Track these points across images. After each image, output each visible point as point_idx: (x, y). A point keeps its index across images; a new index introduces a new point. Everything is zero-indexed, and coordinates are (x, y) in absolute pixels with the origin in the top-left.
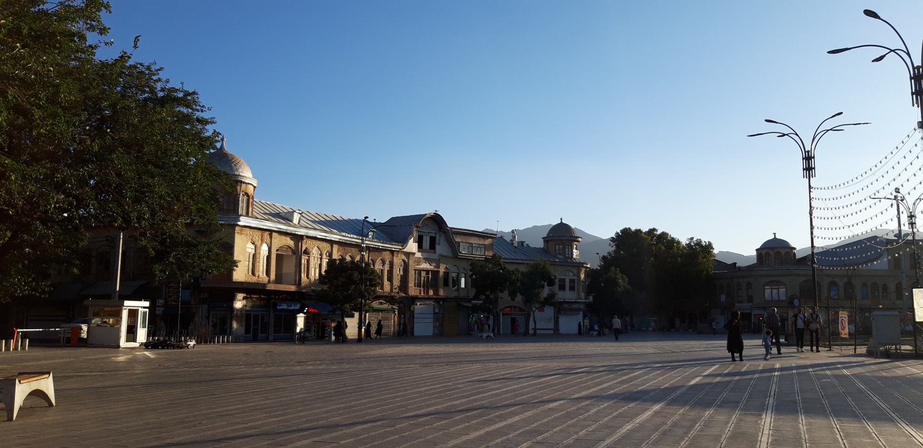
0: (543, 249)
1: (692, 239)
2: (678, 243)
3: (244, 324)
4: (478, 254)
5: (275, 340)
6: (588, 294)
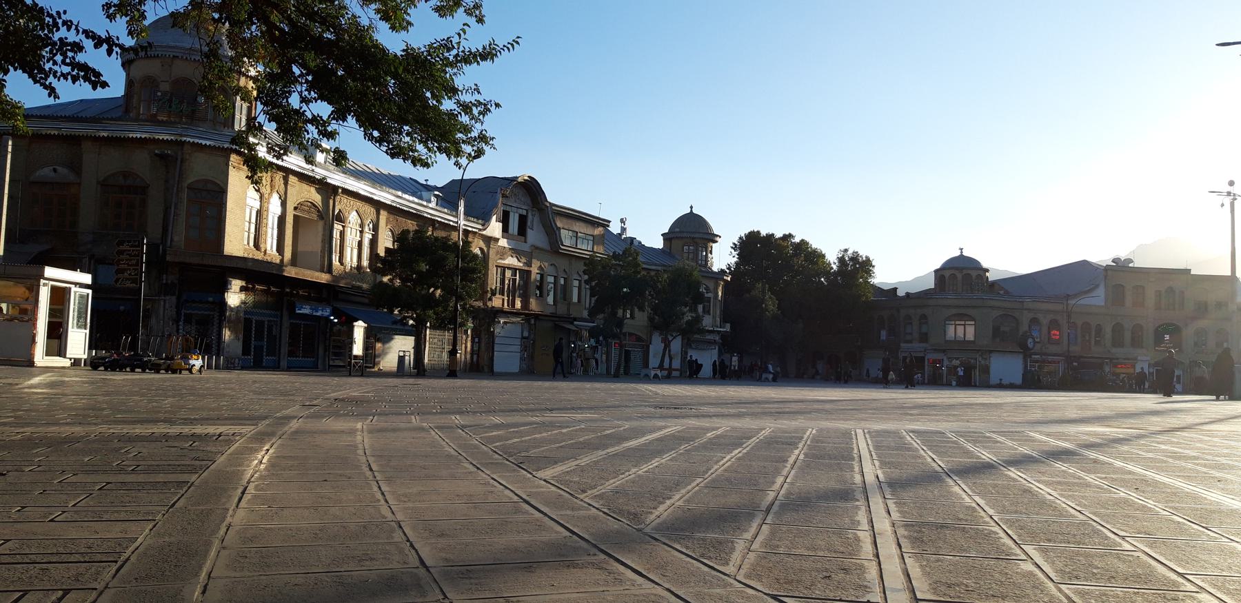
1: (846, 250)
2: (816, 257)
3: (241, 336)
4: (585, 247)
5: (290, 368)
6: (725, 320)
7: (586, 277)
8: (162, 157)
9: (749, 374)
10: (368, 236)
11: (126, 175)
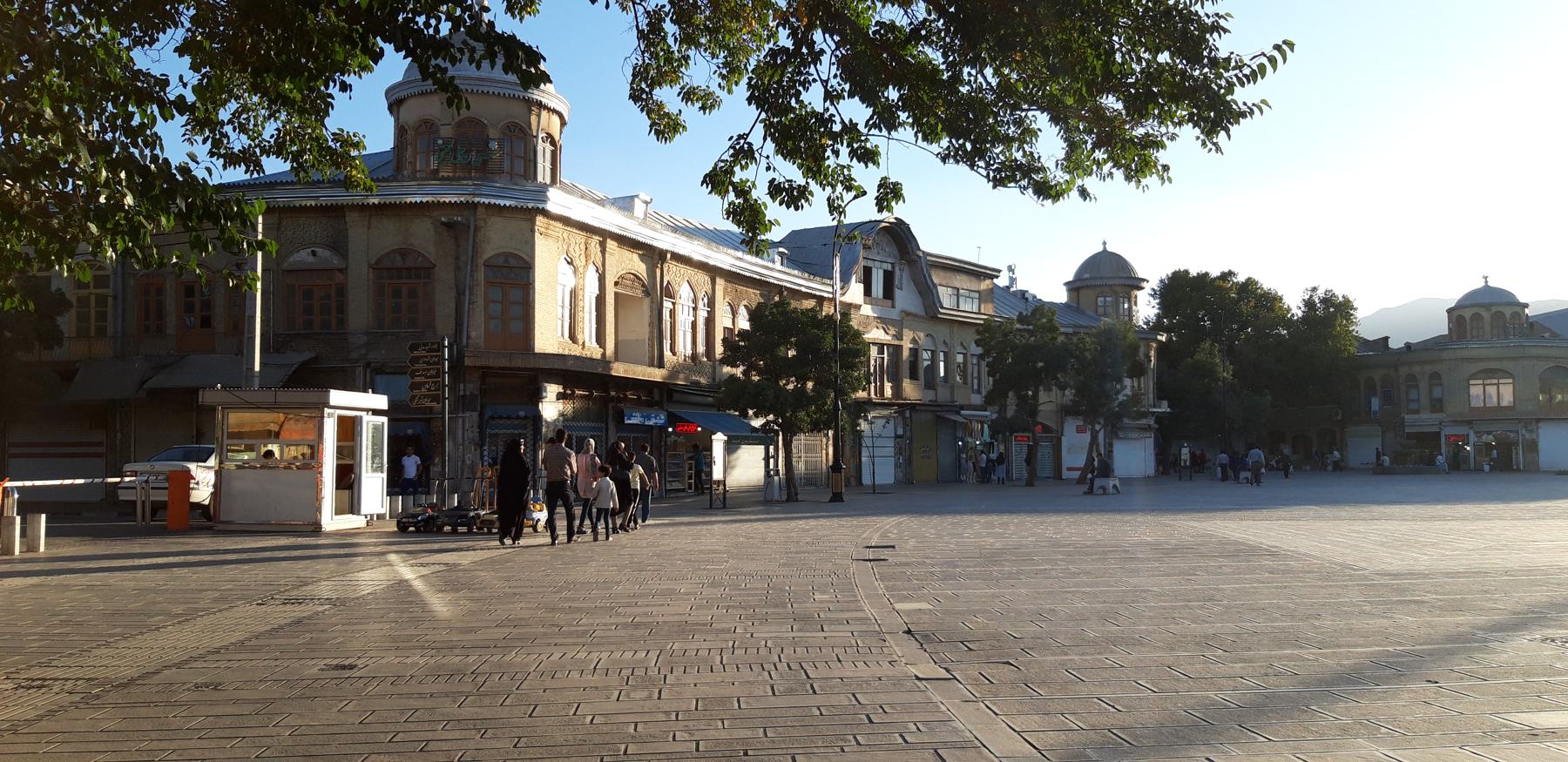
0: (1065, 305)
1: (1314, 289)
2: (1270, 301)
7: (979, 351)
8: (449, 226)
10: (703, 314)
11: (403, 253)
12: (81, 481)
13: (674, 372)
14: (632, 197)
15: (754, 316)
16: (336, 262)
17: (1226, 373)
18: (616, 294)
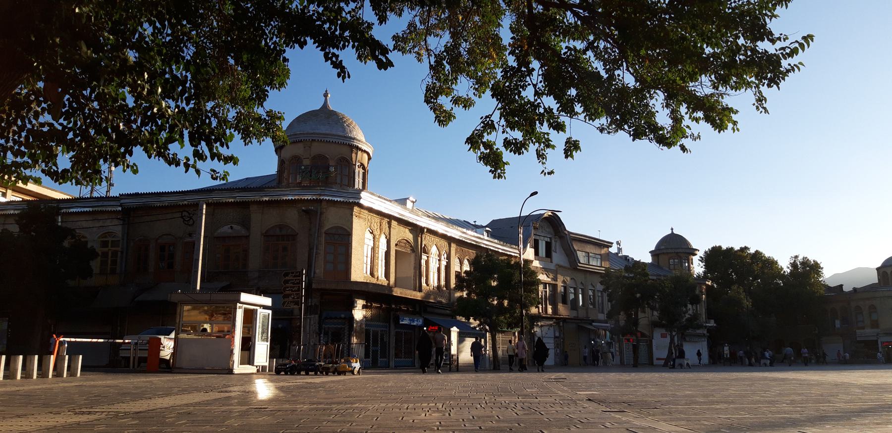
1: (796, 257)
2: (771, 264)
8: (307, 212)
9: (734, 362)
10: (444, 263)
11: (281, 227)
12: (102, 340)
13: (428, 294)
14: (406, 199)
15: (471, 263)
16: (244, 232)
17: (747, 303)
18: (396, 251)
